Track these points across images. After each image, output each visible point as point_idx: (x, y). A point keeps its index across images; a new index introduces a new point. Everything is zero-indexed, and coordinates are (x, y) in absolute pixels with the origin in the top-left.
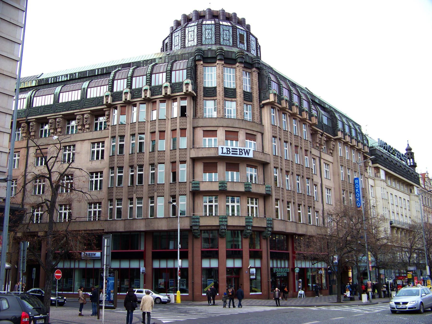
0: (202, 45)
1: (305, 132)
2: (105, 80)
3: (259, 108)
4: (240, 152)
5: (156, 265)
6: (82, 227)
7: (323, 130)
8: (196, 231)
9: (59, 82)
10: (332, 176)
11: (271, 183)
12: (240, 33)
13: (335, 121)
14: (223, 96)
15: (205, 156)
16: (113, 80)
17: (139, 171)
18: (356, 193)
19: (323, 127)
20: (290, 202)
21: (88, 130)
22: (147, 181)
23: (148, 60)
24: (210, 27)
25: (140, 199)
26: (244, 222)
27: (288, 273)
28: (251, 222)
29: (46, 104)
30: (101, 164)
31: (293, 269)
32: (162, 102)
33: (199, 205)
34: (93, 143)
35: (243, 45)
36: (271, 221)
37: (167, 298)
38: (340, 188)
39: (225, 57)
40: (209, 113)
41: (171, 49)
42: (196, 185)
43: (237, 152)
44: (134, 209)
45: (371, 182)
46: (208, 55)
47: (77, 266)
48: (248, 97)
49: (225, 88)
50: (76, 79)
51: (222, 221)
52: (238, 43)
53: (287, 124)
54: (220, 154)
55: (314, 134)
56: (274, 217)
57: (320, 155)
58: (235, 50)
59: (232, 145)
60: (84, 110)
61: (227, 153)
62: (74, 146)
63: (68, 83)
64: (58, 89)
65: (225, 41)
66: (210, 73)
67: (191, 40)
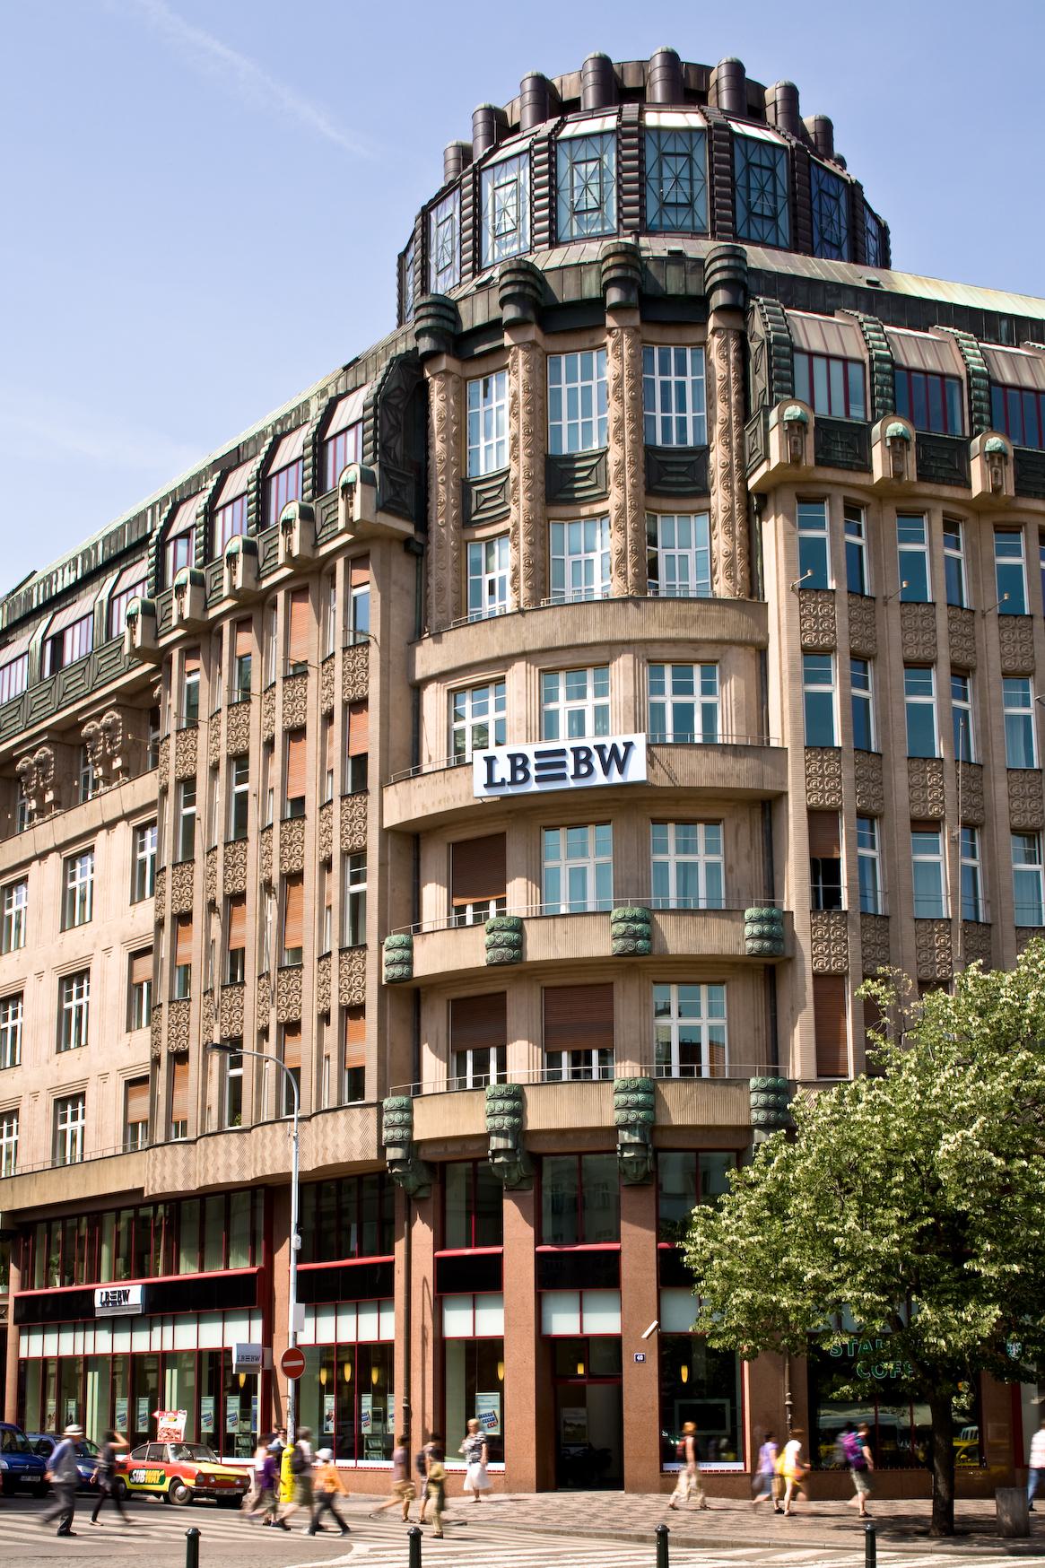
0: (554, 242)
4: (578, 762)
15: (432, 811)
61: (514, 782)
66: (579, 384)
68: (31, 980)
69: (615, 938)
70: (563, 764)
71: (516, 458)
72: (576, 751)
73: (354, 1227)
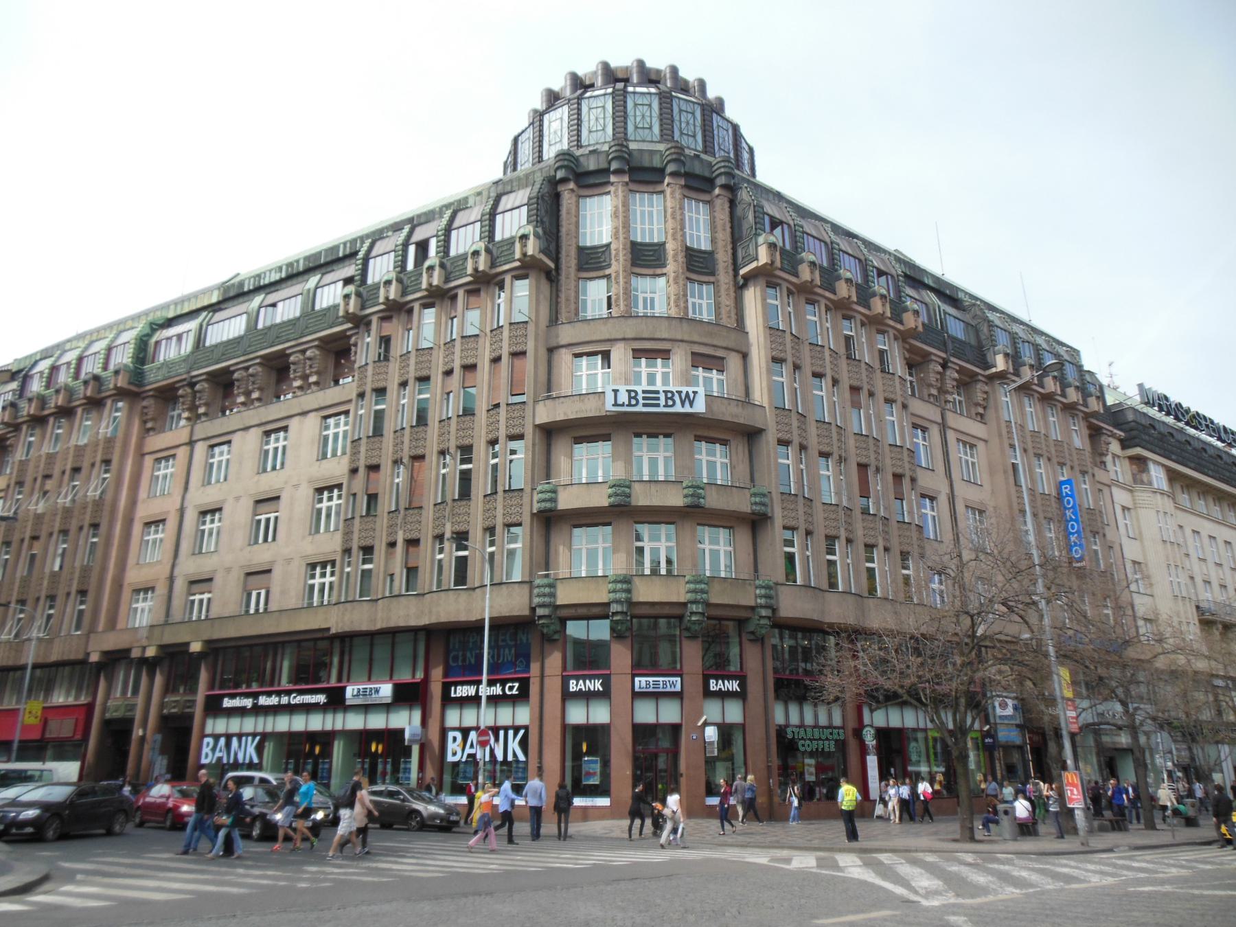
4: (667, 398)
6: (285, 626)
19: (945, 344)
20: (837, 537)
26: (683, 591)
30: (336, 468)
31: (858, 733)
38: (1011, 507)
39: (633, 164)
45: (1121, 497)
47: (339, 727)
48: (698, 264)
49: (634, 244)
53: (819, 325)
54: (609, 406)
56: (780, 576)
60: (304, 339)
61: (630, 405)
68: (230, 500)
69: (686, 496)
70: (658, 399)
71: (617, 238)
73: (336, 660)
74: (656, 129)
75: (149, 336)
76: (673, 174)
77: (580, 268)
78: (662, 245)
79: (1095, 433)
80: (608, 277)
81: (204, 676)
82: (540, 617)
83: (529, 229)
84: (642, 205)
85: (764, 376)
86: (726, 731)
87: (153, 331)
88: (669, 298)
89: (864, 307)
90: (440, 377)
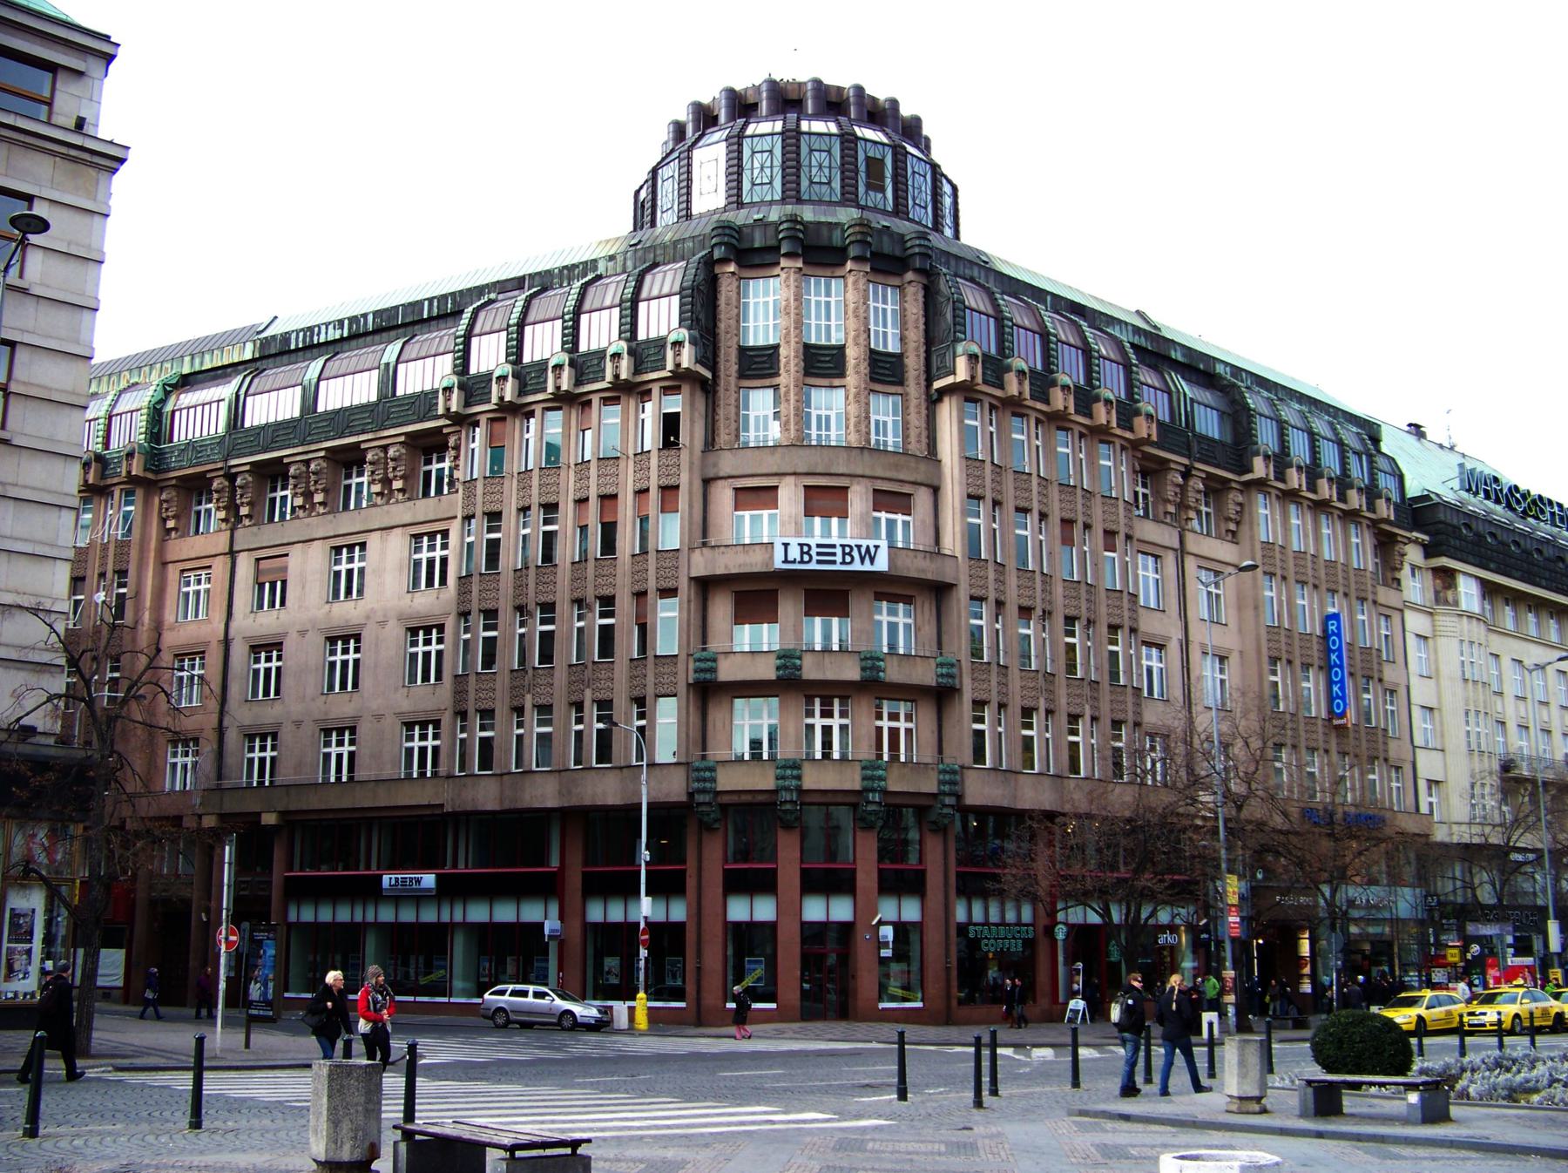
0: (740, 204)
1: (1113, 472)
2: (446, 337)
3: (924, 406)
4: (844, 554)
5: (595, 913)
6: (383, 799)
7: (1189, 457)
8: (704, 808)
9: (320, 345)
10: (1232, 612)
11: (960, 648)
12: (871, 154)
13: (1244, 419)
14: (800, 375)
16: (468, 337)
17: (603, 615)
18: (1331, 668)
19: (1189, 448)
21: (400, 496)
22: (627, 644)
23: (574, 266)
24: (766, 144)
25: (545, 710)
26: (858, 778)
27: (1026, 942)
28: (880, 779)
29: (280, 418)
30: (435, 602)
31: (1049, 931)
32: (606, 401)
33: (719, 724)
34: (417, 537)
35: (880, 196)
36: (954, 772)
37: (594, 1012)
38: (1259, 652)
40: (757, 429)
41: (653, 224)
42: (708, 663)
43: (834, 554)
44: (526, 741)
46: (753, 241)
48: (884, 370)
49: (807, 347)
50: (366, 334)
51: (783, 778)
52: (862, 189)
54: (778, 563)
55: (1149, 471)
56: (967, 757)
57: (1182, 542)
58: (846, 215)
59: (827, 532)
60: (386, 433)
61: (802, 562)
62: (363, 546)
63: (346, 346)
64: (315, 367)
65: (816, 187)
66: (761, 300)
67: (710, 195)
72: (843, 546)
74: (837, 184)
75: (163, 401)
76: (856, 259)
77: (742, 375)
78: (841, 349)
79: (1386, 544)
80: (776, 387)
81: (278, 855)
82: (699, 804)
83: (684, 334)
84: (818, 294)
85: (958, 516)
86: (901, 928)
87: (167, 394)
88: (847, 419)
89: (1085, 415)
90: (571, 505)
